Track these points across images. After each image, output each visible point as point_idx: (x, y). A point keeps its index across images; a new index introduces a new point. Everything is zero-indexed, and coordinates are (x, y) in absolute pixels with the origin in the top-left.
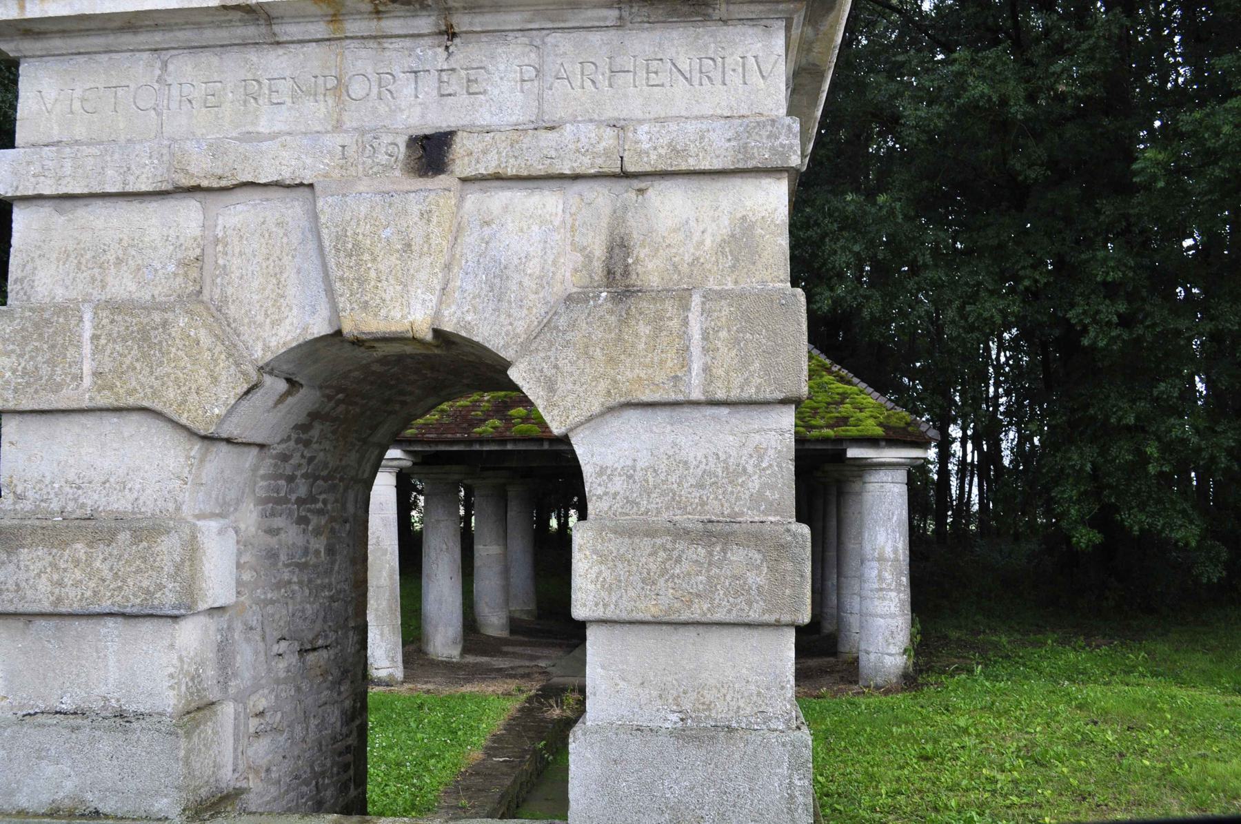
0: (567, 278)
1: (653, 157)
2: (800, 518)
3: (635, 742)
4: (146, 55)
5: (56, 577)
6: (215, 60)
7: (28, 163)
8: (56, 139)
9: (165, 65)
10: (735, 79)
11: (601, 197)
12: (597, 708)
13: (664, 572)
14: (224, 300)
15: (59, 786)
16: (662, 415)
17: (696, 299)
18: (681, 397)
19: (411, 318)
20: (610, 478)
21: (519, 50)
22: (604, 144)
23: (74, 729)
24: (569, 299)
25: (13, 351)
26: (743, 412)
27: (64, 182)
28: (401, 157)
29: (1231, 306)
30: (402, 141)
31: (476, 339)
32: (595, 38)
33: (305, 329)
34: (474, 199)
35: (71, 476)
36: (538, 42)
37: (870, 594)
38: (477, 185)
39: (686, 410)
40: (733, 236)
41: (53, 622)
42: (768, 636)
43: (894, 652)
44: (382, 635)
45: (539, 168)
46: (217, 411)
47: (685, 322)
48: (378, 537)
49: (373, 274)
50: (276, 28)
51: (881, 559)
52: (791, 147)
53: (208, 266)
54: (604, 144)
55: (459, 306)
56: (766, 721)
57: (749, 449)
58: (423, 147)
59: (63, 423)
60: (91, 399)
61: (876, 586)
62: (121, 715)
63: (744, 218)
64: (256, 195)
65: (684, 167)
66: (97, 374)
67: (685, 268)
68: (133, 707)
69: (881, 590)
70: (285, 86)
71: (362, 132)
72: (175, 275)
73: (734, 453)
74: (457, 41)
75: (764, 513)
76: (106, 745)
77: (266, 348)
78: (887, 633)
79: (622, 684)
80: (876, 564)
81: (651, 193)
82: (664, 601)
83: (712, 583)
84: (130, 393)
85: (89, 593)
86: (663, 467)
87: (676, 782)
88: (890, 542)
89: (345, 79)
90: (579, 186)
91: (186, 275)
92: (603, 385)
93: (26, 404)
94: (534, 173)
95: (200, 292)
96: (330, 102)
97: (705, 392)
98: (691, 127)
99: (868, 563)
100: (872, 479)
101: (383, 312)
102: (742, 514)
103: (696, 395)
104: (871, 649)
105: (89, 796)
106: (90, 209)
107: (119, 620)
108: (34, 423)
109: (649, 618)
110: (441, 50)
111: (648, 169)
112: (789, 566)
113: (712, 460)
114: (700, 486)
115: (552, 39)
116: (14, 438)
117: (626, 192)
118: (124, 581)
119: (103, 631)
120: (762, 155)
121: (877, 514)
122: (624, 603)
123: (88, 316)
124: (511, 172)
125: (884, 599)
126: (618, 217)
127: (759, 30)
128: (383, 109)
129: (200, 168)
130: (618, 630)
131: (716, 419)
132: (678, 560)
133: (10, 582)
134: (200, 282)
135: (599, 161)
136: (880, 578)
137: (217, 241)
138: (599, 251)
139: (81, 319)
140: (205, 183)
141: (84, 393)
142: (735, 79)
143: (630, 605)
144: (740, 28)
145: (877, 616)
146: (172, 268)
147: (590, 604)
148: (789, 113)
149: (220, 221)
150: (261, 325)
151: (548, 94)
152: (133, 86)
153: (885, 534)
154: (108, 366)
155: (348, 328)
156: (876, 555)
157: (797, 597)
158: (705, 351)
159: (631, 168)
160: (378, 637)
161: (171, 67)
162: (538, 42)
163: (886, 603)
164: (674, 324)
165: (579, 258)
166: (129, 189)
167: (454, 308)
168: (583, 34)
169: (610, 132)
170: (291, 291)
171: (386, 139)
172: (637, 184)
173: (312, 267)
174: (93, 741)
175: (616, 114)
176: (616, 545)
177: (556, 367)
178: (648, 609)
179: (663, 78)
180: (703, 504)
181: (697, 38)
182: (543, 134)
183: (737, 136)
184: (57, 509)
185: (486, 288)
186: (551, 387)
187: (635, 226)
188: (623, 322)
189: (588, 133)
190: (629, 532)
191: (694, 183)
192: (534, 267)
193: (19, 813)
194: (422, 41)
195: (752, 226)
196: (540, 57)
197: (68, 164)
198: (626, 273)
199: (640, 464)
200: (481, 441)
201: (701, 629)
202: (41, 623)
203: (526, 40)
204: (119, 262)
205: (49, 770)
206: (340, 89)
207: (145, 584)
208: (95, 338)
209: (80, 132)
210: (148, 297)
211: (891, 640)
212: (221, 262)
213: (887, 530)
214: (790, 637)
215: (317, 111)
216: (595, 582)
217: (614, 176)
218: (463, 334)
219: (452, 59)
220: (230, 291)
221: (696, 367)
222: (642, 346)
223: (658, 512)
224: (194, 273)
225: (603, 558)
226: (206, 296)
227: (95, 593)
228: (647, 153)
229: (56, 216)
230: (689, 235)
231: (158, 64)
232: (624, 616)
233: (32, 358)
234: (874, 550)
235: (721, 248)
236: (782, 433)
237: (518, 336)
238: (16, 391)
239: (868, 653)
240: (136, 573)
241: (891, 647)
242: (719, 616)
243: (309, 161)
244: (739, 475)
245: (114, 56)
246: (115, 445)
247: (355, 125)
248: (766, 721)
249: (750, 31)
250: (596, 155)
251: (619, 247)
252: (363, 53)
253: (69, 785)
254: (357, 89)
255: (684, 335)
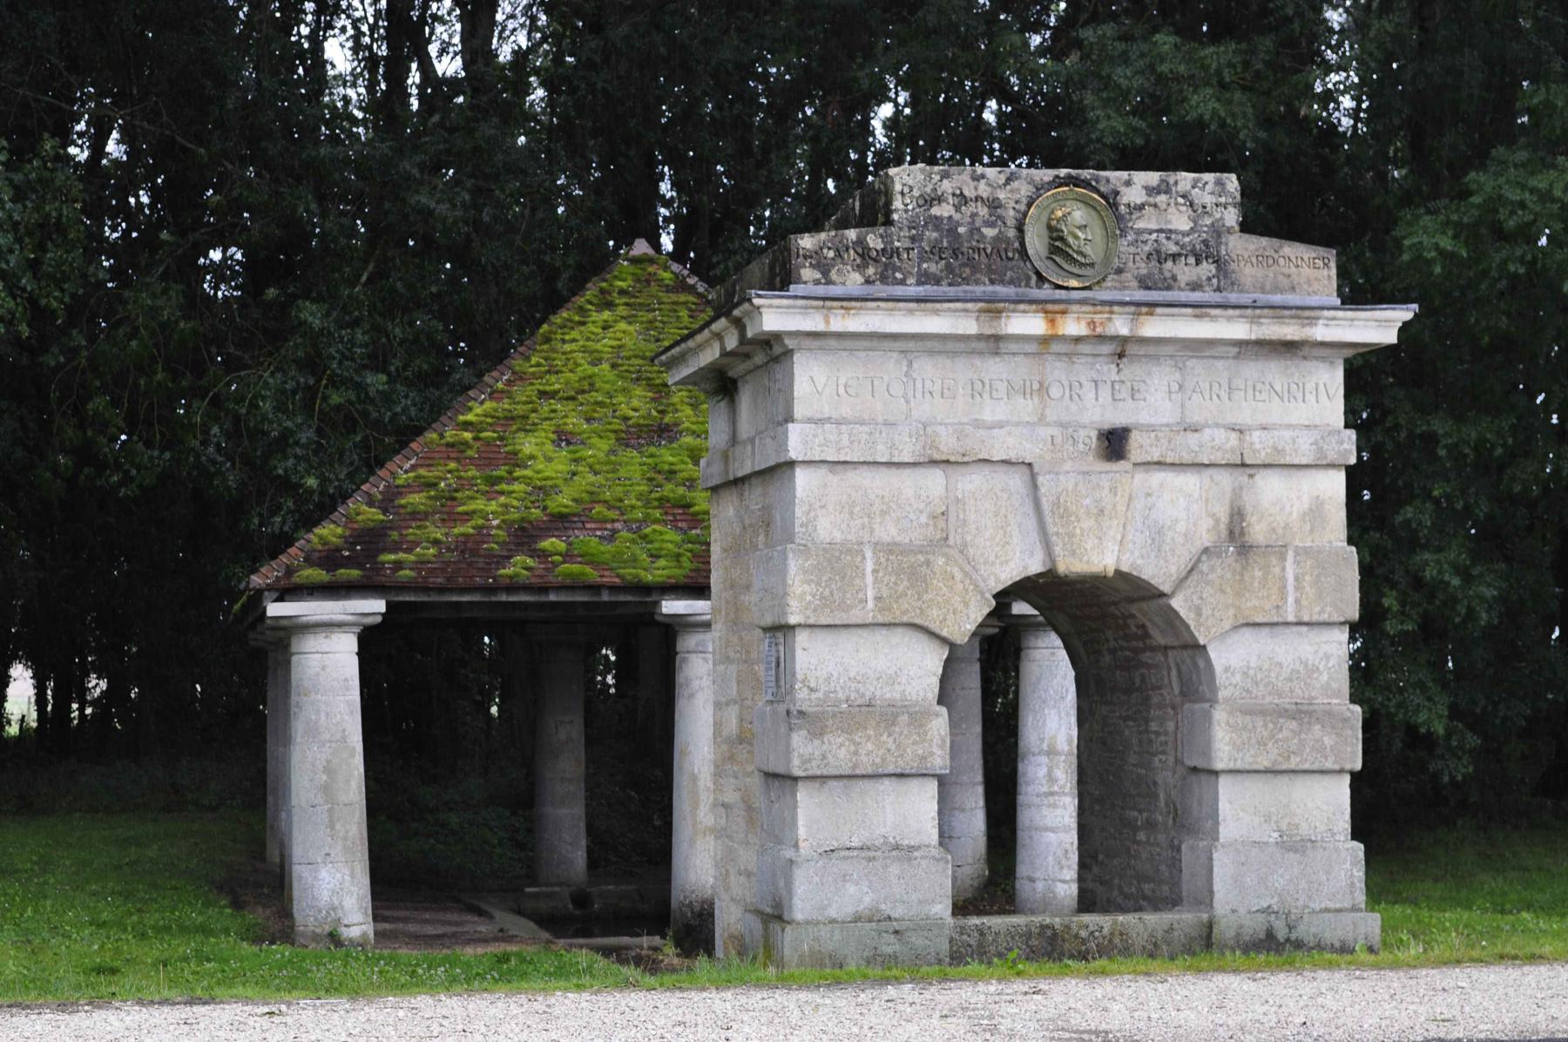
0: (1205, 538)
1: (1263, 454)
2: (1353, 701)
3: (1255, 851)
4: (895, 355)
5: (852, 748)
6: (948, 362)
7: (814, 436)
8: (826, 416)
9: (910, 364)
10: (1311, 398)
11: (1226, 479)
12: (1227, 831)
13: (1272, 736)
14: (966, 545)
15: (860, 901)
16: (1266, 631)
17: (1290, 555)
18: (1281, 620)
19: (1104, 563)
20: (1233, 674)
21: (1168, 369)
22: (1230, 443)
23: (870, 860)
24: (1206, 550)
25: (812, 581)
26: (1316, 630)
27: (843, 452)
28: (1093, 446)
29: (1492, 422)
30: (1094, 434)
31: (1143, 577)
32: (1220, 364)
33: (1025, 568)
34: (1140, 477)
35: (852, 674)
36: (1180, 365)
37: (1036, 800)
38: (1142, 468)
39: (1281, 628)
40: (1311, 509)
41: (842, 783)
42: (1326, 781)
43: (1068, 878)
44: (352, 875)
45: (1187, 458)
46: (968, 627)
47: (1283, 569)
48: (344, 730)
49: (1078, 531)
50: (1001, 345)
51: (1052, 752)
52: (1351, 451)
53: (952, 518)
54: (1230, 443)
55: (1132, 553)
56: (1333, 835)
57: (1321, 654)
58: (1108, 439)
59: (844, 635)
60: (874, 617)
61: (1045, 789)
62: (897, 847)
63: (1318, 497)
64: (987, 469)
65: (1282, 462)
66: (878, 599)
67: (1280, 531)
68: (906, 842)
69: (1052, 794)
70: (1002, 387)
71: (1063, 425)
72: (927, 525)
73: (1311, 657)
74: (1125, 360)
75: (1329, 697)
76: (894, 869)
77: (997, 580)
78: (1060, 853)
79: (1241, 814)
80: (1044, 759)
81: (1257, 477)
82: (1272, 757)
83: (1302, 743)
84: (905, 612)
85: (878, 760)
86: (1266, 666)
87: (1282, 876)
88: (1063, 728)
89: (1046, 385)
90: (1210, 471)
91: (935, 526)
92: (1231, 612)
93: (824, 621)
94: (1185, 462)
95: (947, 539)
96: (1036, 400)
97: (1296, 616)
98: (1288, 434)
99: (1032, 759)
100: (1040, 643)
101: (1085, 559)
102: (1316, 698)
103: (1291, 618)
104: (1038, 875)
105: (883, 907)
106: (857, 472)
107: (893, 779)
108: (821, 635)
109: (1262, 768)
110: (1113, 366)
111: (1259, 462)
112: (1349, 732)
113: (1298, 663)
114: (1290, 680)
115: (1189, 363)
116: (806, 645)
117: (1241, 477)
118: (905, 750)
119: (882, 788)
120: (1332, 456)
121: (1046, 691)
122: (1249, 759)
123: (869, 554)
124: (1169, 460)
125: (1055, 806)
126: (1237, 493)
127: (1327, 365)
128: (1074, 407)
129: (947, 445)
130: (1239, 777)
131: (1300, 634)
132: (1281, 730)
133: (817, 753)
134: (946, 530)
135: (1228, 456)
136: (1051, 779)
137: (958, 500)
138: (1224, 519)
139: (864, 558)
140: (952, 459)
141: (869, 612)
142: (1311, 398)
143: (1251, 760)
144: (1315, 363)
145: (1047, 829)
146: (923, 519)
147: (1226, 760)
148: (1347, 426)
149: (959, 485)
150: (993, 563)
151: (1188, 404)
152: (886, 378)
153: (1057, 718)
154: (885, 592)
155: (1062, 569)
156: (1045, 746)
157: (1354, 753)
158: (1297, 589)
159: (1248, 462)
160: (347, 878)
161: (915, 366)
162: (1180, 365)
163: (1059, 812)
164: (1277, 570)
165: (1211, 522)
166: (896, 460)
167: (1128, 555)
168: (1211, 361)
169: (1234, 435)
170: (1016, 539)
171: (1082, 433)
172: (1249, 471)
173: (1031, 523)
174: (886, 867)
175: (1234, 421)
176: (1241, 720)
177: (1201, 598)
178: (1264, 762)
179: (1264, 396)
180: (1292, 691)
181: (1287, 367)
182: (1189, 434)
183: (1315, 443)
184: (843, 698)
185: (1149, 542)
186: (1199, 613)
187: (1248, 501)
188: (1244, 568)
189: (1221, 435)
190: (1248, 712)
191: (1286, 472)
192: (1181, 527)
193: (830, 922)
194: (1100, 359)
195: (1322, 504)
196: (1182, 375)
197: (845, 438)
198: (1242, 533)
199: (1253, 665)
200: (512, 588)
201: (1292, 775)
202: (833, 783)
203: (1172, 363)
204: (883, 513)
205: (851, 889)
206: (1043, 389)
207: (920, 752)
208: (875, 571)
209: (846, 411)
210: (907, 541)
211: (1064, 862)
212: (961, 516)
213: (1060, 713)
214: (1347, 779)
215: (1026, 407)
216: (1228, 744)
217: (1236, 466)
218: (1135, 573)
219: (1122, 374)
220: (968, 538)
221: (1291, 599)
222: (1256, 585)
223: (1263, 696)
224: (941, 524)
225: (1233, 728)
226: (951, 541)
227: (884, 760)
228: (1259, 451)
229: (830, 476)
230: (1282, 509)
231: (905, 363)
232: (1248, 767)
233: (827, 586)
234: (1042, 740)
235: (1303, 516)
236: (1341, 644)
237: (1171, 575)
238: (815, 610)
239: (1032, 880)
240: (913, 744)
241: (1065, 871)
242: (1307, 766)
243: (1028, 446)
244: (1313, 672)
245: (871, 353)
246: (886, 651)
247: (1055, 419)
248: (1333, 835)
249: (1322, 365)
250: (1226, 451)
251: (1237, 515)
252: (1058, 364)
253: (867, 900)
254: (1055, 392)
255: (1283, 579)
